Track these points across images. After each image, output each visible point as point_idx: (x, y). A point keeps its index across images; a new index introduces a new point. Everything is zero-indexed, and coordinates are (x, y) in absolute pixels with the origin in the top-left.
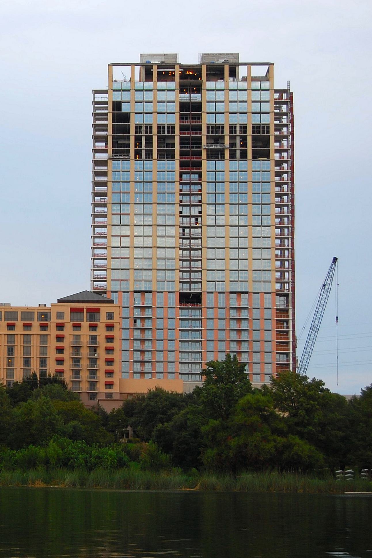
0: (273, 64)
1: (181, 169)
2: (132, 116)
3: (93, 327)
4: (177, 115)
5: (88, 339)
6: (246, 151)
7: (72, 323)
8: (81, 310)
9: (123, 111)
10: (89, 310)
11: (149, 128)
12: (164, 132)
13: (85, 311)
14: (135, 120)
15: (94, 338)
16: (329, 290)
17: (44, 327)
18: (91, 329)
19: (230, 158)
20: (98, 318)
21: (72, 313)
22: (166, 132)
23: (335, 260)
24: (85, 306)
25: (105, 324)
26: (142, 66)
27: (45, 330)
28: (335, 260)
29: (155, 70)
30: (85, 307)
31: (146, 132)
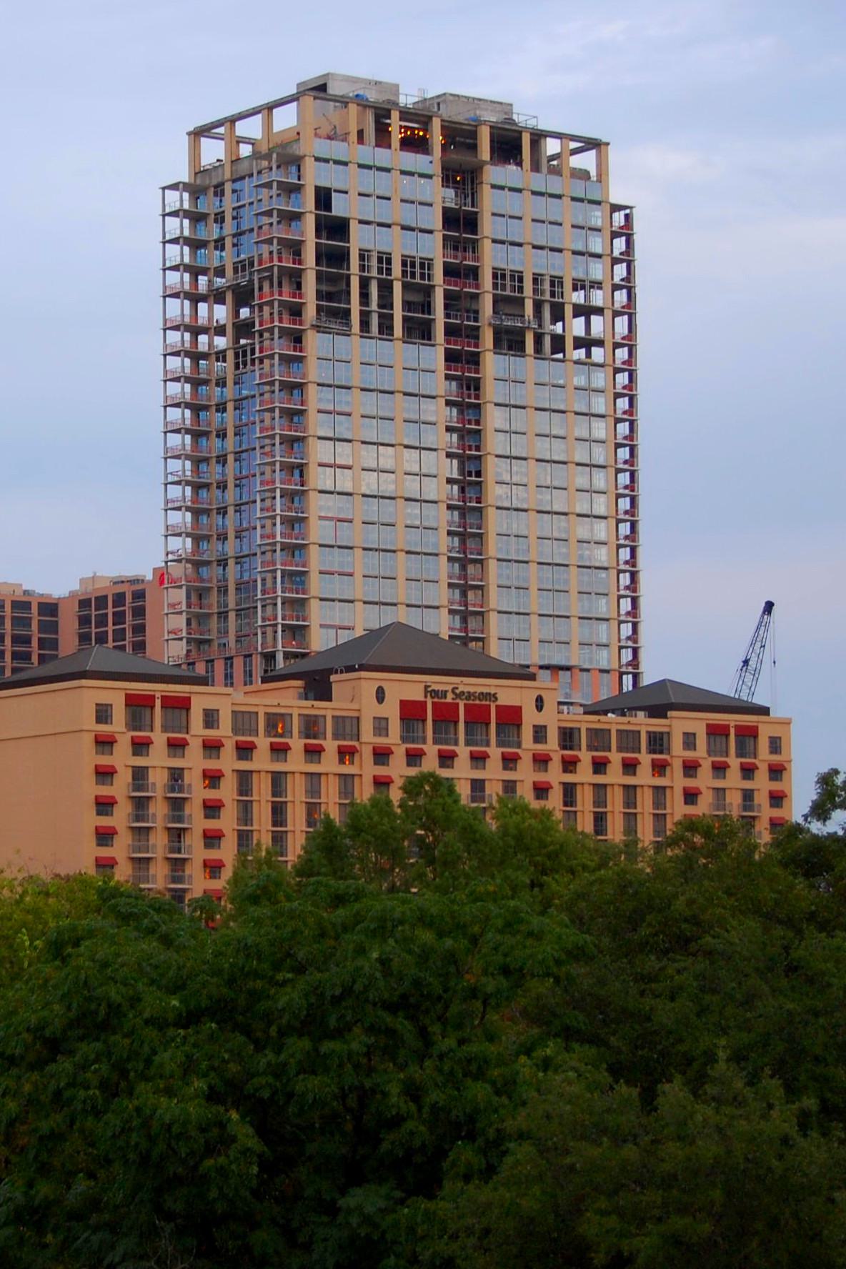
0: (608, 144)
1: (448, 368)
2: (354, 226)
3: (176, 746)
4: (439, 237)
5: (499, 788)
6: (361, 304)
7: (405, 746)
8: (148, 701)
9: (334, 213)
10: (169, 703)
11: (385, 259)
12: (504, 289)
13: (158, 703)
14: (359, 239)
15: (176, 776)
16: (756, 672)
17: (346, 754)
18: (100, 749)
19: (495, 346)
20: (321, 730)
21: (712, 738)
22: (418, 275)
23: (769, 607)
24: (158, 689)
25: (200, 740)
26: (365, 107)
27: (383, 764)
28: (769, 607)
29: (395, 123)
30: (732, 724)
31: (380, 271)
